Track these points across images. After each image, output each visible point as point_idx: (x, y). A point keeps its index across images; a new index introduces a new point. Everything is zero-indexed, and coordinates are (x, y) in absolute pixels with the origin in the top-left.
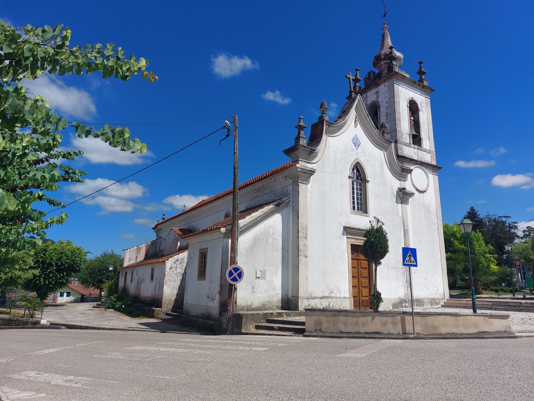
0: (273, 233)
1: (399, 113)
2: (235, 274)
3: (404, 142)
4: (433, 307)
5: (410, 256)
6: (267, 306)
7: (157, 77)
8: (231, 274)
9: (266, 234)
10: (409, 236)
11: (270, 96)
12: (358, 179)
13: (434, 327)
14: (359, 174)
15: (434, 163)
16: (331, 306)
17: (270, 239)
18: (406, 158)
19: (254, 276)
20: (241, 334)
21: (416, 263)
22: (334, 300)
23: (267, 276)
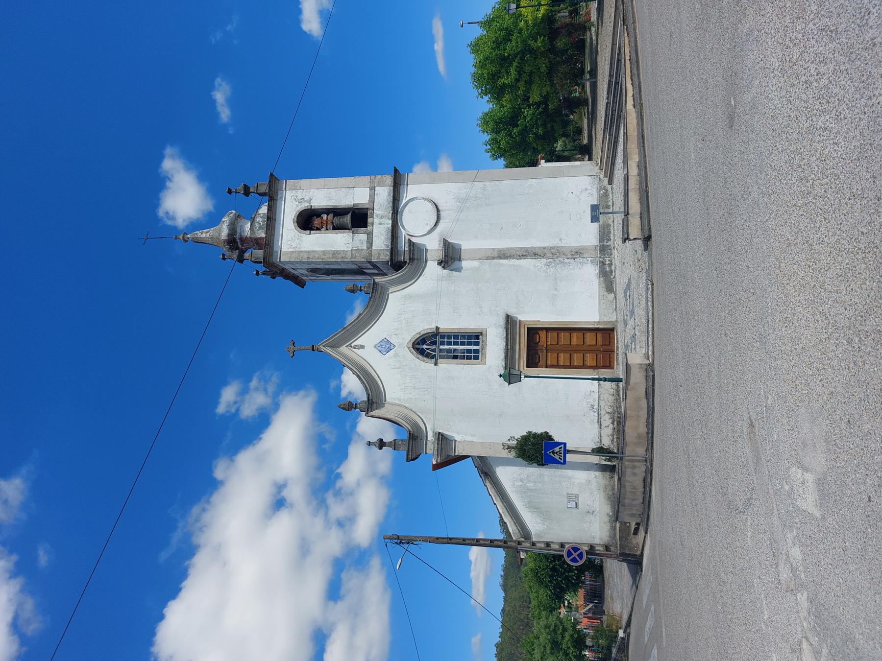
0: (521, 480)
1: (324, 252)
2: (575, 555)
3: (368, 248)
4: (610, 203)
5: (553, 453)
6: (610, 493)
7: (184, 199)
8: (574, 560)
9: (524, 491)
10: (508, 249)
11: (225, 114)
12: (434, 343)
13: (639, 436)
14: (429, 345)
15: (389, 180)
16: (609, 411)
17: (529, 485)
18: (392, 249)
19: (575, 511)
20: (642, 555)
21: (561, 443)
22: (602, 404)
23: (574, 493)
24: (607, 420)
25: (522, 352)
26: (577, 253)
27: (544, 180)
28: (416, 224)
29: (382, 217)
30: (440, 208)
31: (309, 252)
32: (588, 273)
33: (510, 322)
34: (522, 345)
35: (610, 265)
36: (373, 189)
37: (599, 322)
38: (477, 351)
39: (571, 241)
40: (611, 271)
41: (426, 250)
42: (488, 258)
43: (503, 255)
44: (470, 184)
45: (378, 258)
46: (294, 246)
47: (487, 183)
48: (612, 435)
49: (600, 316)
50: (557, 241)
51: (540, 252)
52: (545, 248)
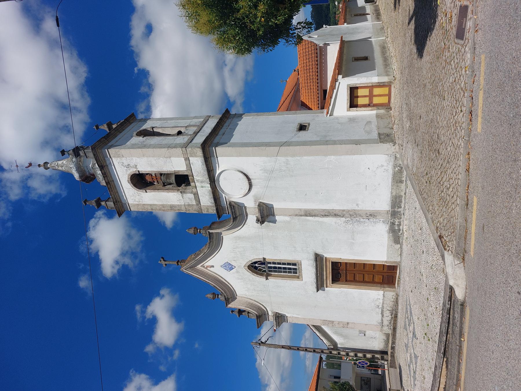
3: (197, 205)
10: (313, 210)
14: (259, 268)
22: (385, 306)
24: (387, 314)
25: (328, 275)
26: (372, 215)
27: (343, 157)
28: (233, 190)
29: (202, 182)
30: (250, 177)
31: (151, 205)
32: (380, 230)
33: (318, 259)
34: (328, 272)
35: (399, 225)
36: (187, 159)
37: (386, 262)
38: (296, 269)
39: (367, 206)
40: (399, 230)
41: (245, 207)
42: (296, 215)
43: (308, 213)
44: (273, 159)
45: (207, 211)
46: (137, 200)
47: (289, 158)
48: (391, 320)
49: (388, 258)
50: (355, 205)
51: (339, 214)
52: (344, 211)
